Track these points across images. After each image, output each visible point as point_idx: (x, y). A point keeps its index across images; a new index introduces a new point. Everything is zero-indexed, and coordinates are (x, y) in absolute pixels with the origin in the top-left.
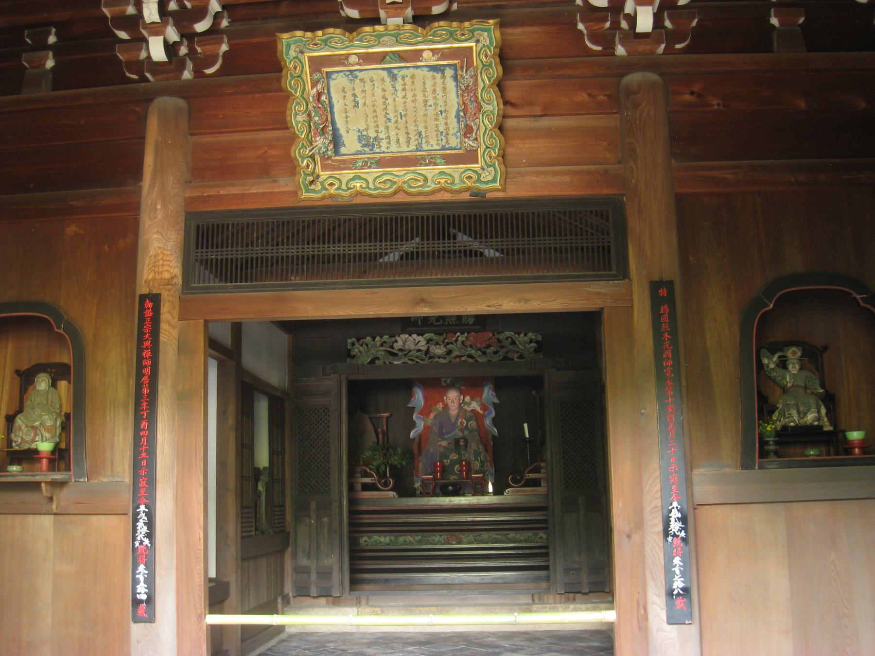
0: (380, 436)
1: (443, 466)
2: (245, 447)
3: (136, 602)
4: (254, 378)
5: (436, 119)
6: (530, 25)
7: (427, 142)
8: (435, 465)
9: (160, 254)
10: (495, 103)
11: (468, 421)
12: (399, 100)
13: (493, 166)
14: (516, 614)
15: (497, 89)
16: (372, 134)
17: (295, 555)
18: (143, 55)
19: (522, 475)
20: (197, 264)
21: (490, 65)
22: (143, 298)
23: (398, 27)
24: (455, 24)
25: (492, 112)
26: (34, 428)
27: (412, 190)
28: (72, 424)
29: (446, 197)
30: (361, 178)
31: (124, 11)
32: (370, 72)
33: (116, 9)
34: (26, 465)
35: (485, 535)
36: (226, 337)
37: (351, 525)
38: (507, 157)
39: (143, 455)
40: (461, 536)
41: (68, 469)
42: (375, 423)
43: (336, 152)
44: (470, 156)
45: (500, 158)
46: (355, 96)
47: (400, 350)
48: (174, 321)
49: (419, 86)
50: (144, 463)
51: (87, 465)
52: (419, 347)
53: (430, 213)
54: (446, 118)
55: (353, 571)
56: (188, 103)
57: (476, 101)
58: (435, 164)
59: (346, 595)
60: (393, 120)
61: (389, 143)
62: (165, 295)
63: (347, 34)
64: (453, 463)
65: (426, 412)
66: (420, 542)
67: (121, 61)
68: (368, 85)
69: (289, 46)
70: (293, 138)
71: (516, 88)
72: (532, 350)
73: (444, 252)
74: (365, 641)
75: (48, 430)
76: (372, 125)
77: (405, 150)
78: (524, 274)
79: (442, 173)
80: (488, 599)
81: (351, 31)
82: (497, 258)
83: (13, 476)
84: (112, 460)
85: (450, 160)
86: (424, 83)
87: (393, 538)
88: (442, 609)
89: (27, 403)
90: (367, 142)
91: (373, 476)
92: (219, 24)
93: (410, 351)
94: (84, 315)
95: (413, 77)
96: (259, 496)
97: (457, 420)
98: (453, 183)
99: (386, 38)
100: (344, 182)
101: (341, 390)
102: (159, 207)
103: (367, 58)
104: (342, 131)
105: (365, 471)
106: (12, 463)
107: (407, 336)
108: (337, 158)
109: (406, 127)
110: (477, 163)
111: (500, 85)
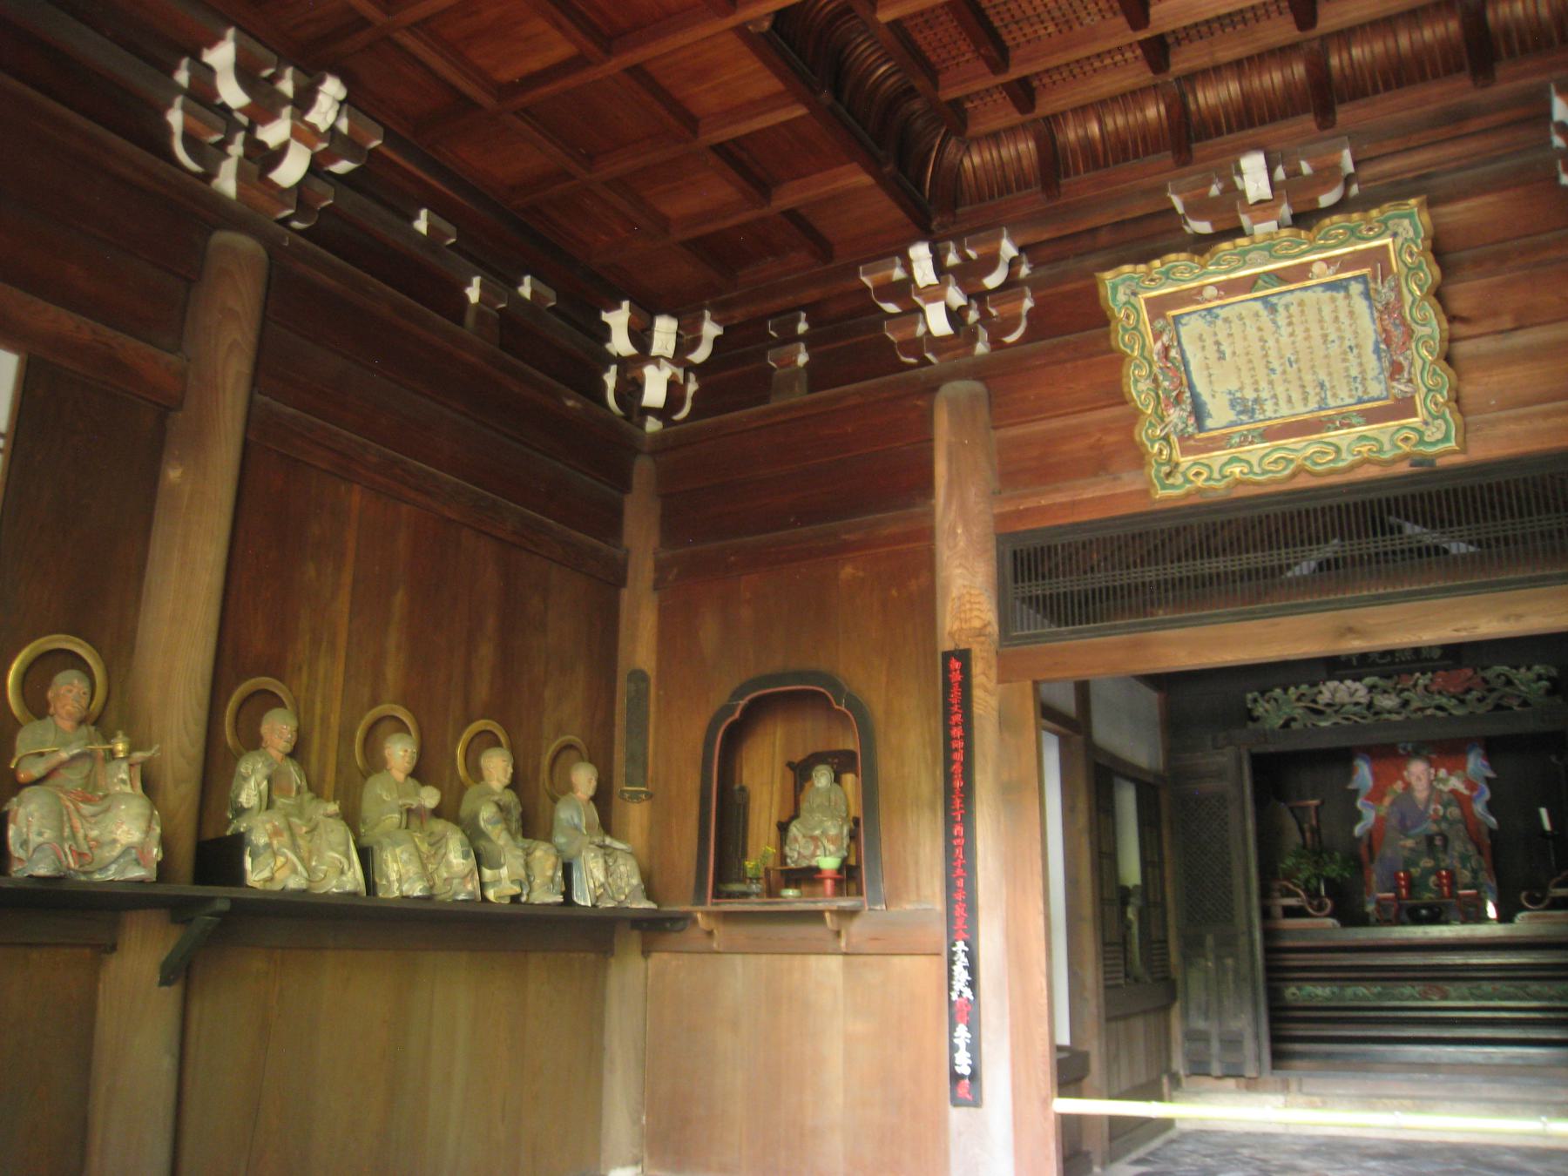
0: (1308, 835)
1: (1409, 877)
2: (1104, 856)
3: (955, 1078)
4: (1115, 759)
5: (1344, 360)
6: (1478, 195)
7: (1334, 395)
8: (1397, 877)
9: (967, 593)
10: (1434, 322)
11: (1445, 806)
12: (1285, 339)
13: (1442, 417)
14: (1544, 1119)
15: (1434, 300)
16: (1250, 395)
17: (1185, 1015)
18: (920, 330)
19: (1544, 889)
20: (1018, 603)
21: (1419, 267)
22: (947, 656)
23: (1270, 236)
24: (1356, 216)
25: (1431, 337)
26: (815, 839)
27: (1319, 468)
28: (863, 831)
29: (1373, 472)
30: (1240, 460)
31: (890, 277)
32: (1236, 307)
33: (880, 275)
34: (806, 889)
35: (1487, 987)
36: (1066, 702)
37: (1269, 969)
38: (1464, 401)
39: (959, 871)
40: (1449, 988)
41: (859, 892)
42: (1299, 815)
43: (1200, 427)
44: (1404, 407)
45: (1453, 404)
46: (1218, 343)
47: (1329, 705)
48: (992, 685)
49: (1311, 315)
50: (960, 883)
51: (884, 888)
52: (1356, 699)
53: (1351, 499)
54: (1359, 356)
55: (1276, 1039)
56: (988, 388)
57: (1404, 323)
58: (1350, 426)
59: (1267, 1075)
60: (1279, 370)
61: (1276, 404)
62: (977, 651)
63: (1196, 258)
64: (1427, 873)
65: (1376, 796)
66: (1379, 996)
67: (892, 343)
68: (1236, 325)
69: (1115, 288)
70: (1136, 415)
71: (1464, 296)
72: (1542, 692)
73: (1377, 554)
74: (1297, 1148)
75: (833, 841)
76: (1248, 381)
77: (1303, 410)
78: (1511, 576)
79: (1362, 438)
80: (1500, 1091)
81: (1201, 253)
82: (1473, 555)
83: (789, 903)
84: (917, 880)
85: (1371, 417)
86: (1320, 310)
87: (1336, 990)
88: (1421, 1104)
89: (804, 806)
90: (1245, 408)
91: (1297, 895)
92: (1017, 273)
93: (1343, 705)
94: (869, 681)
95: (1301, 304)
96: (1129, 927)
97: (1427, 807)
98: (1380, 451)
99: (1252, 255)
100: (1216, 468)
101: (1240, 769)
102: (959, 531)
103: (1230, 288)
104: (1205, 396)
105: (1288, 889)
106: (787, 886)
107: (1336, 683)
108: (1203, 435)
109: (1300, 378)
110: (1415, 414)
111: (1439, 294)
